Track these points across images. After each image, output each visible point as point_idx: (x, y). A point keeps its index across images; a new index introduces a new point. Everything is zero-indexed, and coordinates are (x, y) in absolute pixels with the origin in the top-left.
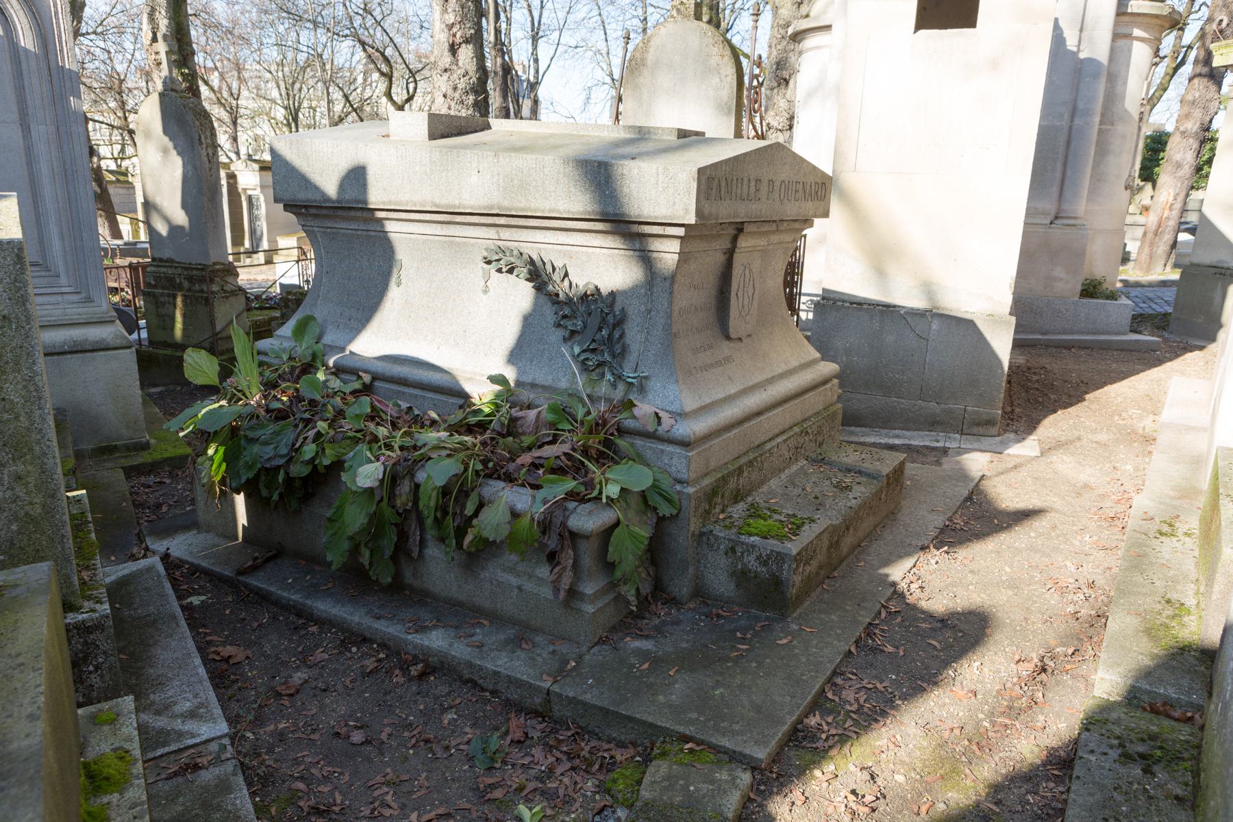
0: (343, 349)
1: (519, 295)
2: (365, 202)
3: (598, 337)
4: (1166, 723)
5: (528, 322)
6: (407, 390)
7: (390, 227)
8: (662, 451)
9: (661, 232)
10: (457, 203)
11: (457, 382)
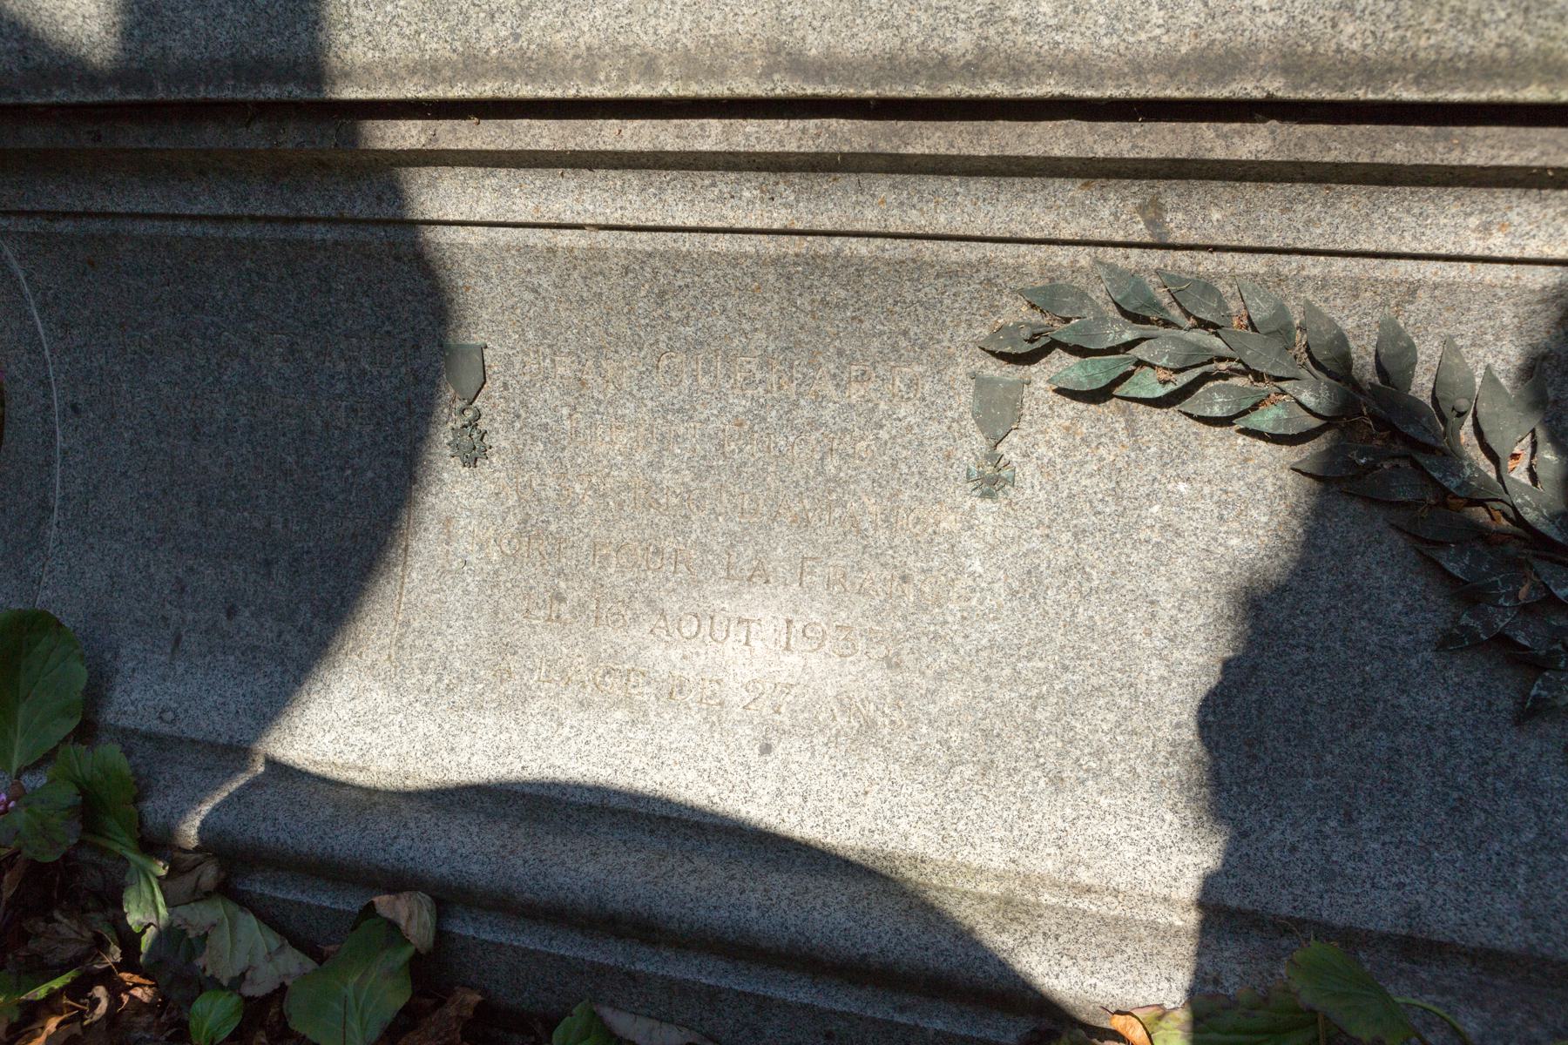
0: (236, 753)
1: (1221, 505)
2: (314, 69)
6: (647, 962)
7: (442, 198)
10: (963, 42)
11: (965, 937)
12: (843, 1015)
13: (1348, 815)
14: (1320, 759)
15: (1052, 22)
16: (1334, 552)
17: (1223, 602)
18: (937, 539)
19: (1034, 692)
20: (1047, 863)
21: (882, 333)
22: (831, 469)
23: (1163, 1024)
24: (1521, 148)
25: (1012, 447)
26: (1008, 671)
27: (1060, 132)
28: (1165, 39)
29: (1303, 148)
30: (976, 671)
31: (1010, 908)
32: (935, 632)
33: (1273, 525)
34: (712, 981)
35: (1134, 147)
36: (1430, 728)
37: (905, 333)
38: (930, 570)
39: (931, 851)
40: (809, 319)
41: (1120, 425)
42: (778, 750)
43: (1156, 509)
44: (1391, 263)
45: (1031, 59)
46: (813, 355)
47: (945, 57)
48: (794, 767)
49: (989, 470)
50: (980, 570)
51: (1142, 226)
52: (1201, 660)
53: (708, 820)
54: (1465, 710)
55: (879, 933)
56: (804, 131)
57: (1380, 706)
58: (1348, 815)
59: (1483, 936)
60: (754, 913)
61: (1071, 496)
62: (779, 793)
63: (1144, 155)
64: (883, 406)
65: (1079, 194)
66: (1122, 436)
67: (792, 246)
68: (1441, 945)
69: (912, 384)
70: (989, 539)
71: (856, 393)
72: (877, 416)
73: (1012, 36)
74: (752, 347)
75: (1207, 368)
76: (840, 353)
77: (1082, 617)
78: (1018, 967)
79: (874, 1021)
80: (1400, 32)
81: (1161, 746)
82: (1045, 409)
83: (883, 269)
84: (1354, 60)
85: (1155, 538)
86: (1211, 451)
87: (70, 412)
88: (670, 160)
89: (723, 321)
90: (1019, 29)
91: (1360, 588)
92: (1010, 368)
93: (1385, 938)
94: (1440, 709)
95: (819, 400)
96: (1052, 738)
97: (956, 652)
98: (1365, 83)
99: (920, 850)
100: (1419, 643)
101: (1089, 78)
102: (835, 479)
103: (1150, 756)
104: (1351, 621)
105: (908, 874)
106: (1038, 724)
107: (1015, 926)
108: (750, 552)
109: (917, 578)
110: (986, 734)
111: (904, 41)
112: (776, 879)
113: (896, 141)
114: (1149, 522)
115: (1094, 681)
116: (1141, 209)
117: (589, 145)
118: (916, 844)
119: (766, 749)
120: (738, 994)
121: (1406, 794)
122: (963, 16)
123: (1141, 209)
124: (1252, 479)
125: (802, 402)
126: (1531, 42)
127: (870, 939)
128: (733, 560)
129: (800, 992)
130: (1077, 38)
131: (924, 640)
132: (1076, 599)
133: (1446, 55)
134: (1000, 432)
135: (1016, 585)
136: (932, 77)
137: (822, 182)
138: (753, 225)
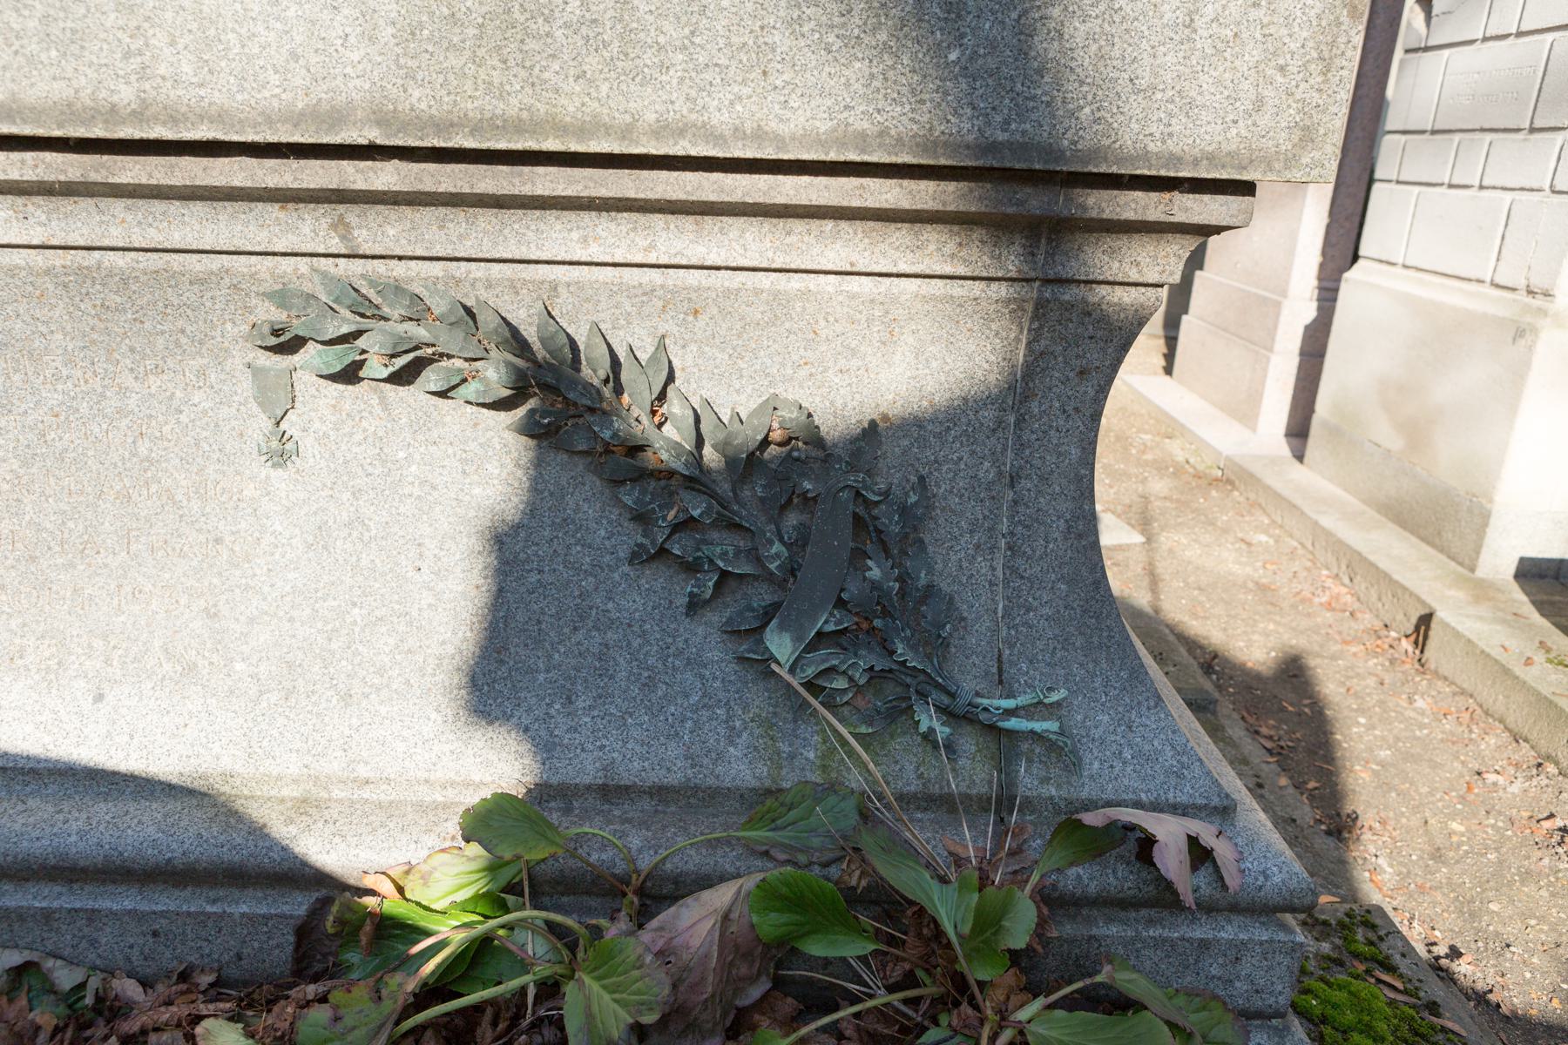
1: (473, 461)
3: (853, 590)
4: (1210, 766)
5: (514, 552)
8: (1204, 945)
9: (1154, 215)
10: (125, 95)
11: (258, 832)
12: (163, 914)
13: (569, 698)
14: (550, 657)
15: (194, 80)
16: (551, 494)
17: (473, 540)
18: (242, 505)
19: (329, 627)
20: (333, 765)
21: (163, 333)
22: (143, 450)
23: (410, 877)
24: (570, 183)
25: (292, 424)
26: (308, 611)
27: (236, 167)
28: (284, 96)
29: (421, 181)
30: (281, 614)
31: (305, 806)
32: (247, 585)
33: (504, 475)
34: (44, 904)
35: (296, 179)
36: (630, 626)
37: (183, 331)
38: (238, 532)
39: (238, 768)
40: (96, 321)
41: (375, 401)
42: (109, 698)
43: (414, 468)
44: (532, 266)
45: (184, 109)
46: (110, 352)
47: (114, 106)
48: (124, 711)
49: (275, 444)
50: (280, 529)
51: (337, 240)
52: (460, 588)
53: (42, 765)
54: (654, 608)
55: (187, 838)
56: (23, 162)
57: (594, 612)
58: (569, 698)
59: (655, 777)
60: (73, 838)
61: (346, 462)
62: (109, 735)
63: (304, 186)
64: (178, 394)
65: (282, 215)
66: (378, 410)
67: (58, 259)
68: (627, 788)
69: (202, 373)
70: (284, 502)
71: (154, 382)
72: (176, 403)
73: (164, 90)
74: (53, 346)
75: (418, 353)
76: (132, 350)
77: (365, 562)
78: (297, 850)
79: (189, 914)
80: (452, 97)
81: (430, 660)
82: (313, 391)
83: (143, 278)
84: (425, 118)
85: (417, 492)
86: (448, 419)
87: (1259, 791)
88: (801, 211)
89: (19, 325)
90: (169, 84)
91: (573, 521)
92: (278, 358)
93: (589, 788)
94: (636, 610)
95: (123, 391)
96: (344, 663)
97: (265, 599)
98: (438, 134)
99: (229, 767)
100: (618, 559)
101: (233, 126)
102: (147, 459)
103: (421, 669)
104: (568, 547)
105: (223, 789)
106: (333, 654)
107: (304, 818)
108: (81, 527)
109: (228, 539)
110: (290, 665)
111: (77, 92)
112: (102, 807)
113: (104, 172)
114: (410, 479)
115: (378, 613)
116: (334, 227)
117: (527, 190)
118: (226, 763)
119: (99, 698)
120: (69, 911)
121: (611, 677)
122: (121, 73)
123: (334, 227)
124: (482, 440)
125: (108, 394)
126: (542, 108)
127: (174, 846)
128: (66, 536)
129: (126, 900)
130: (217, 94)
131: (237, 591)
132: (359, 546)
133: (488, 115)
134: (280, 413)
135: (310, 539)
136: (106, 122)
137: (66, 204)
138: (14, 242)
